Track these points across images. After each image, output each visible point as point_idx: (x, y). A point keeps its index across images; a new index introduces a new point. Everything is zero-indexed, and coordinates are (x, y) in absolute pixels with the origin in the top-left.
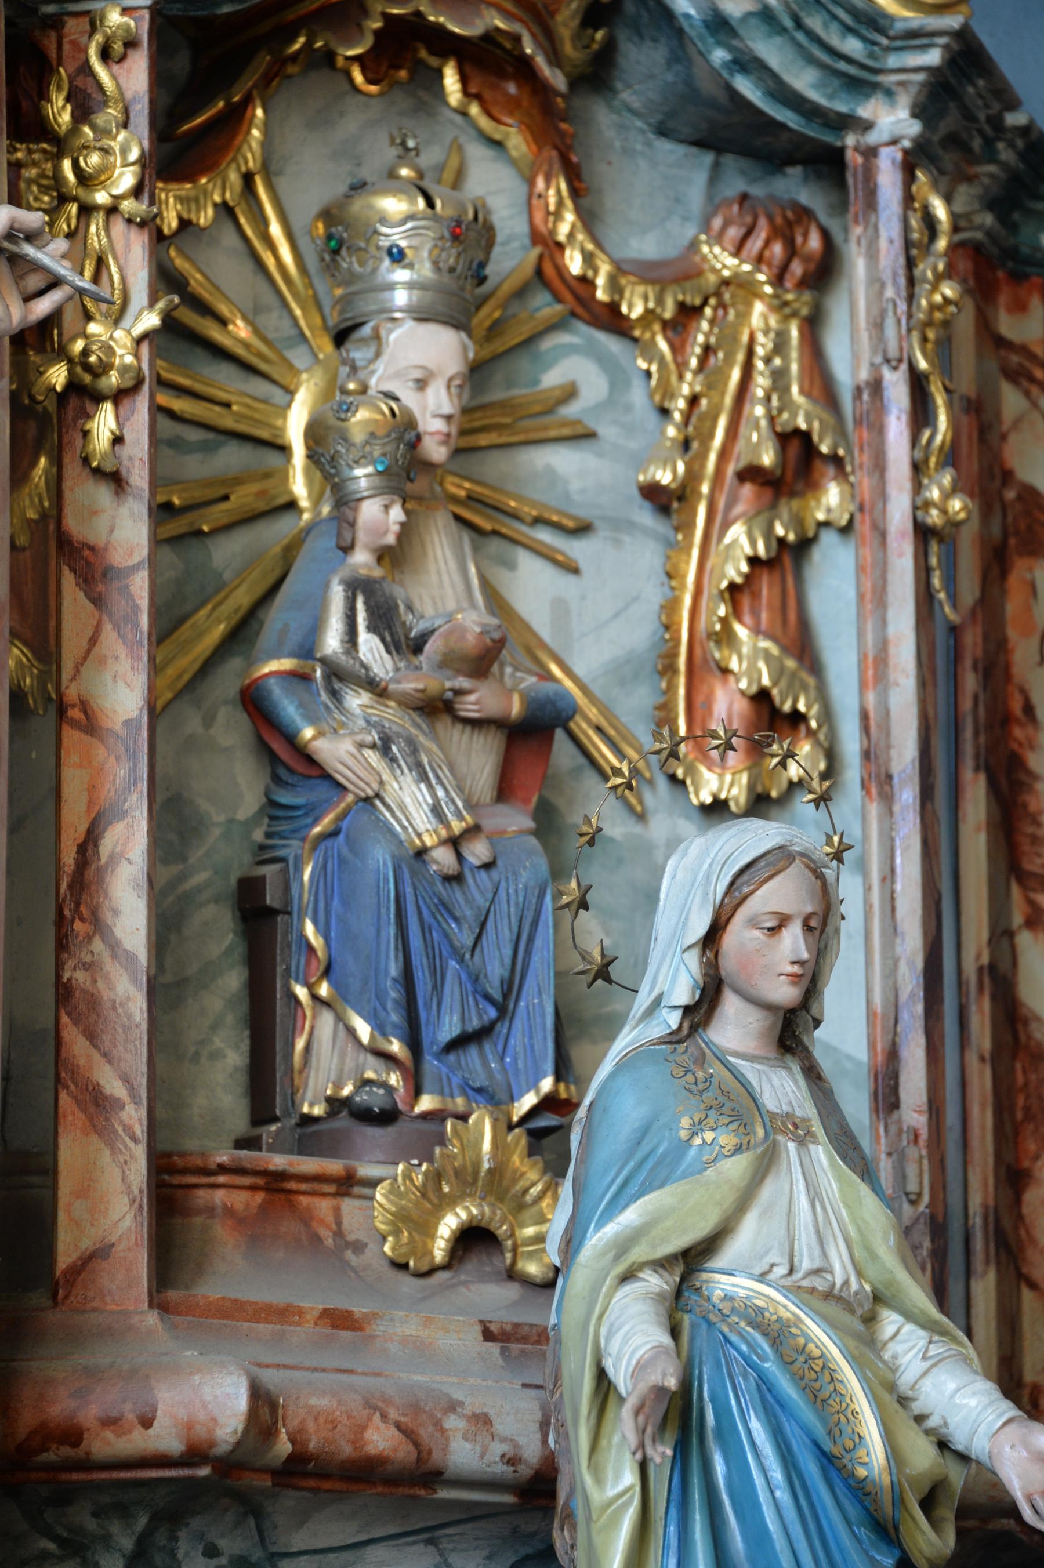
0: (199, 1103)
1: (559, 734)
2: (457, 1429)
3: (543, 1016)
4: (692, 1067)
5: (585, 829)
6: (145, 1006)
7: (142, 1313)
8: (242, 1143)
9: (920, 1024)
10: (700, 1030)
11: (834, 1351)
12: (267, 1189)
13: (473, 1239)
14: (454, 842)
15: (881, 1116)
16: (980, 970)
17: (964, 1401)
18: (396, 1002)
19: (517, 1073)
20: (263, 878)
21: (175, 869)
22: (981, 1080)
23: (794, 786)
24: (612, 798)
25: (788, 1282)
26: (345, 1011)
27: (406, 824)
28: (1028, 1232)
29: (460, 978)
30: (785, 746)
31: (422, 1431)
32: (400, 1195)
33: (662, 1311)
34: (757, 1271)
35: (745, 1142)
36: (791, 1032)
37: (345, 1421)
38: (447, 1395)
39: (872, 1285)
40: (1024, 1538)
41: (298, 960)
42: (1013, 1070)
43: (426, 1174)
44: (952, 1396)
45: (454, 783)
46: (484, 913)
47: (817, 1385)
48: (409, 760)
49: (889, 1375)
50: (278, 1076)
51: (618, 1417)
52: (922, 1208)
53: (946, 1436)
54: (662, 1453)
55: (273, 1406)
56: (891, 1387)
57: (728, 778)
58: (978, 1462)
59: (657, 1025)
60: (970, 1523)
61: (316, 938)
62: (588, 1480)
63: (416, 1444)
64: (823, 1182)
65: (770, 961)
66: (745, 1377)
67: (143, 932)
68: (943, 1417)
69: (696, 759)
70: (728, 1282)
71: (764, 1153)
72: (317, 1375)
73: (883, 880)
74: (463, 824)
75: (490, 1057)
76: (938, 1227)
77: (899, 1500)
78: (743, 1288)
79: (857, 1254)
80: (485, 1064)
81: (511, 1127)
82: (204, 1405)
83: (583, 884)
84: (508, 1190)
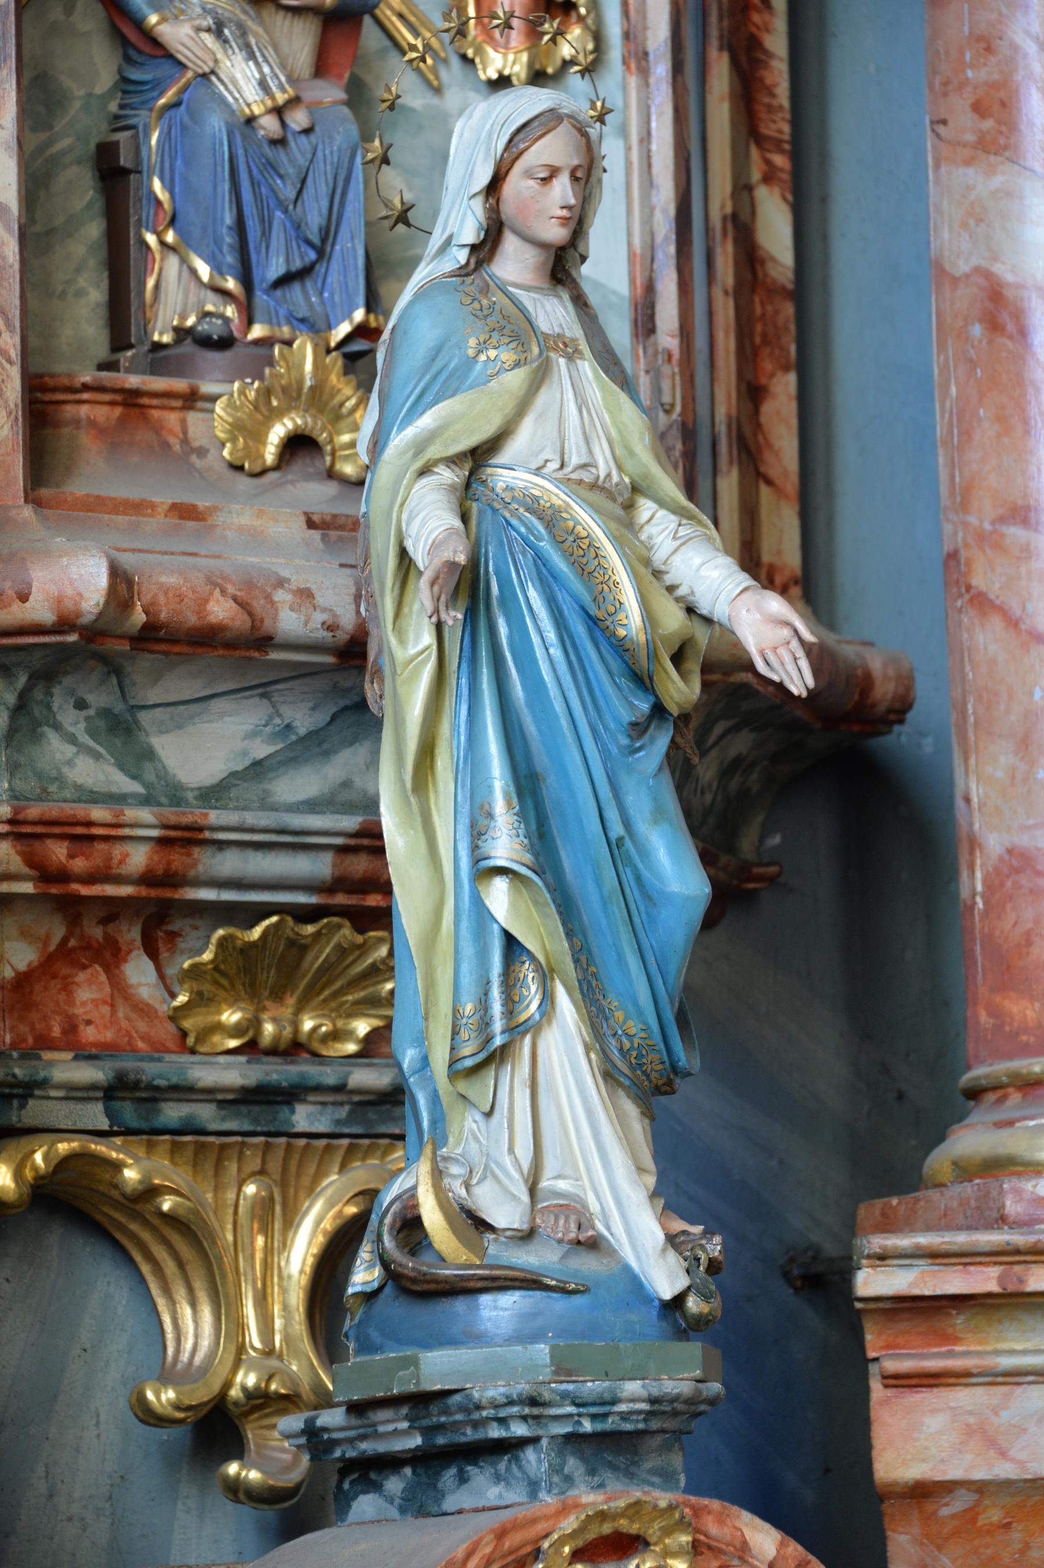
0: (67, 333)
1: (367, 20)
2: (284, 601)
3: (355, 258)
4: (478, 295)
5: (386, 96)
6: (17, 249)
7: (19, 507)
8: (102, 367)
9: (672, 263)
10: (485, 265)
11: (598, 533)
12: (125, 404)
13: (299, 445)
14: (279, 111)
15: (640, 339)
16: (724, 219)
17: (708, 574)
18: (230, 246)
19: (334, 305)
20: (116, 144)
21: (43, 136)
22: (726, 311)
23: (567, 64)
24: (408, 69)
25: (560, 475)
26: (188, 255)
27: (237, 96)
28: (765, 439)
29: (285, 226)
30: (555, 25)
31: (255, 604)
32: (235, 408)
33: (454, 499)
34: (534, 466)
35: (523, 359)
36: (561, 266)
37: (190, 595)
38: (276, 573)
39: (631, 478)
40: (760, 688)
41: (148, 212)
42: (752, 302)
43: (258, 390)
44: (698, 570)
45: (278, 61)
46: (304, 170)
47: (584, 560)
48: (240, 41)
49: (645, 553)
50: (133, 309)
51: (417, 589)
52: (675, 415)
53: (693, 602)
54: (453, 618)
55: (130, 583)
56: (647, 562)
57: (511, 57)
58: (720, 625)
59: (448, 261)
60: (715, 677)
61: (163, 193)
62: (393, 641)
63: (251, 614)
64: (589, 392)
65: (542, 206)
66: (524, 555)
67: (14, 187)
68: (691, 587)
69: (484, 41)
70: (508, 475)
71: (539, 368)
72: (166, 557)
73: (641, 141)
74: (286, 96)
75: (311, 292)
76: (688, 432)
77: (653, 655)
78: (521, 480)
79: (617, 452)
80: (307, 298)
81: (329, 351)
82: (72, 582)
83: (386, 141)
84: (326, 404)
